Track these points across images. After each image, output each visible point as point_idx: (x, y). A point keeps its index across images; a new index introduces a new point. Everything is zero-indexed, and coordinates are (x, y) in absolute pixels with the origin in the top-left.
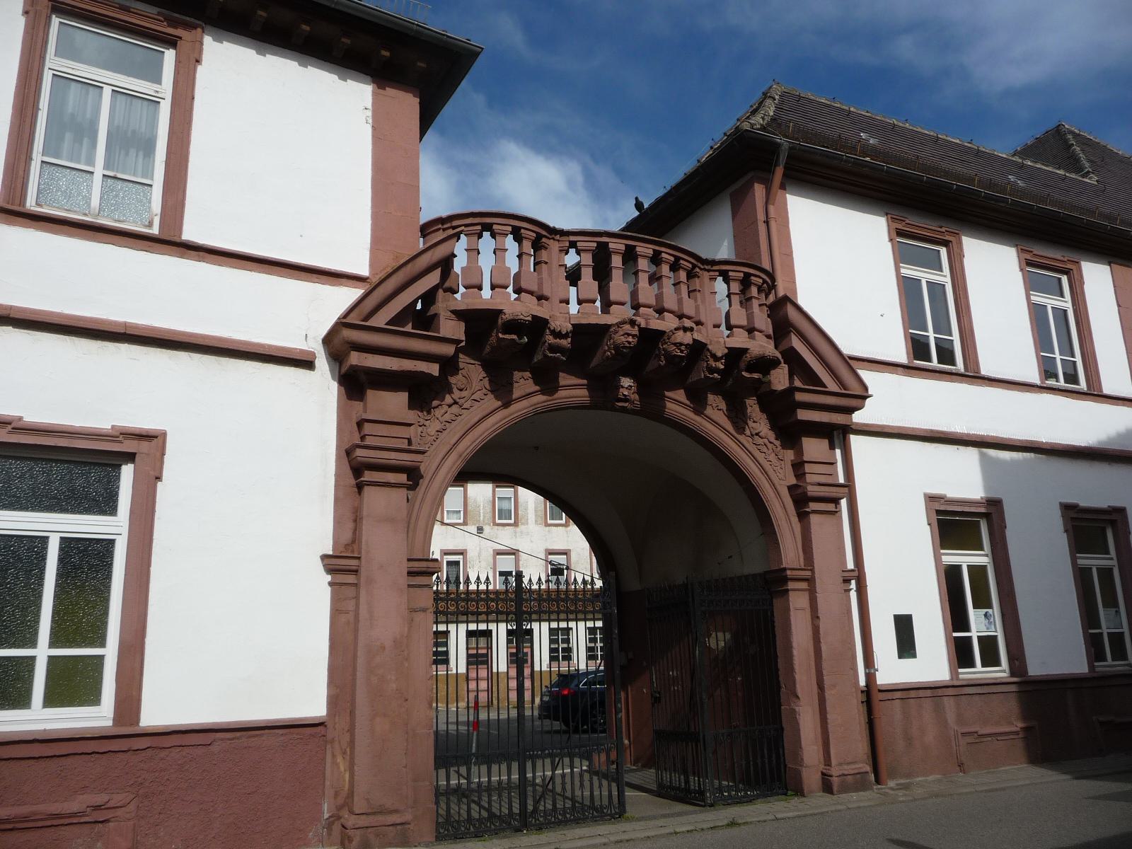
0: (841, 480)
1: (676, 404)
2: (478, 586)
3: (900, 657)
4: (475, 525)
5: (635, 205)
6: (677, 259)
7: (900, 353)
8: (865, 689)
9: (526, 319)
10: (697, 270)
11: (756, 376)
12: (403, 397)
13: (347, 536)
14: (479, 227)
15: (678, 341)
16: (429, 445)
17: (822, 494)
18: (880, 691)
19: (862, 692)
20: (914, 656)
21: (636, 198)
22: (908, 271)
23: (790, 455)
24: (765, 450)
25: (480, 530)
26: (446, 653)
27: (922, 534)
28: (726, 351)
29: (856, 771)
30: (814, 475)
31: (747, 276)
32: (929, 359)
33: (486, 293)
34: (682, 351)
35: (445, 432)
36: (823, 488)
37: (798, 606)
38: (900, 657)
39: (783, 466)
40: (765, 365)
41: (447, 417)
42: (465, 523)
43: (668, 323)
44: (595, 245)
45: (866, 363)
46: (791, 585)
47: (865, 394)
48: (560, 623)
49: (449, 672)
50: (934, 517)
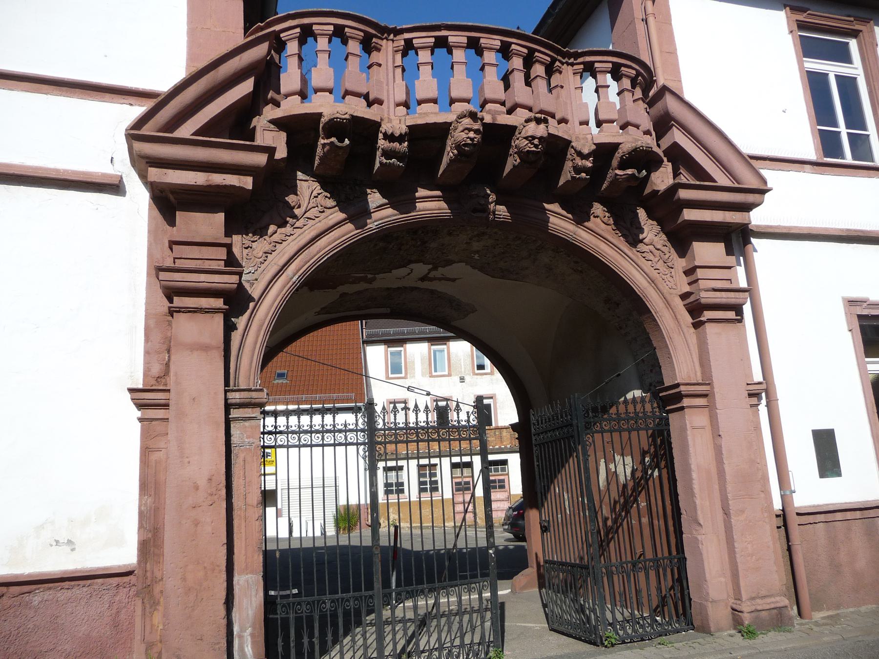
0: (743, 284)
1: (560, 222)
3: (822, 475)
6: (532, 51)
7: (809, 150)
8: (781, 513)
9: (344, 117)
11: (629, 171)
13: (156, 369)
15: (529, 134)
17: (724, 301)
18: (798, 514)
19: (777, 516)
20: (839, 474)
22: (815, 65)
23: (681, 264)
24: (651, 257)
25: (462, 380)
27: (845, 342)
28: (594, 147)
29: (773, 606)
30: (708, 280)
32: (841, 155)
34: (536, 146)
36: (718, 294)
37: (695, 424)
38: (822, 475)
39: (673, 274)
40: (644, 160)
42: (449, 375)
43: (516, 119)
44: (433, 40)
45: (767, 162)
46: (686, 402)
47: (765, 188)
50: (862, 328)
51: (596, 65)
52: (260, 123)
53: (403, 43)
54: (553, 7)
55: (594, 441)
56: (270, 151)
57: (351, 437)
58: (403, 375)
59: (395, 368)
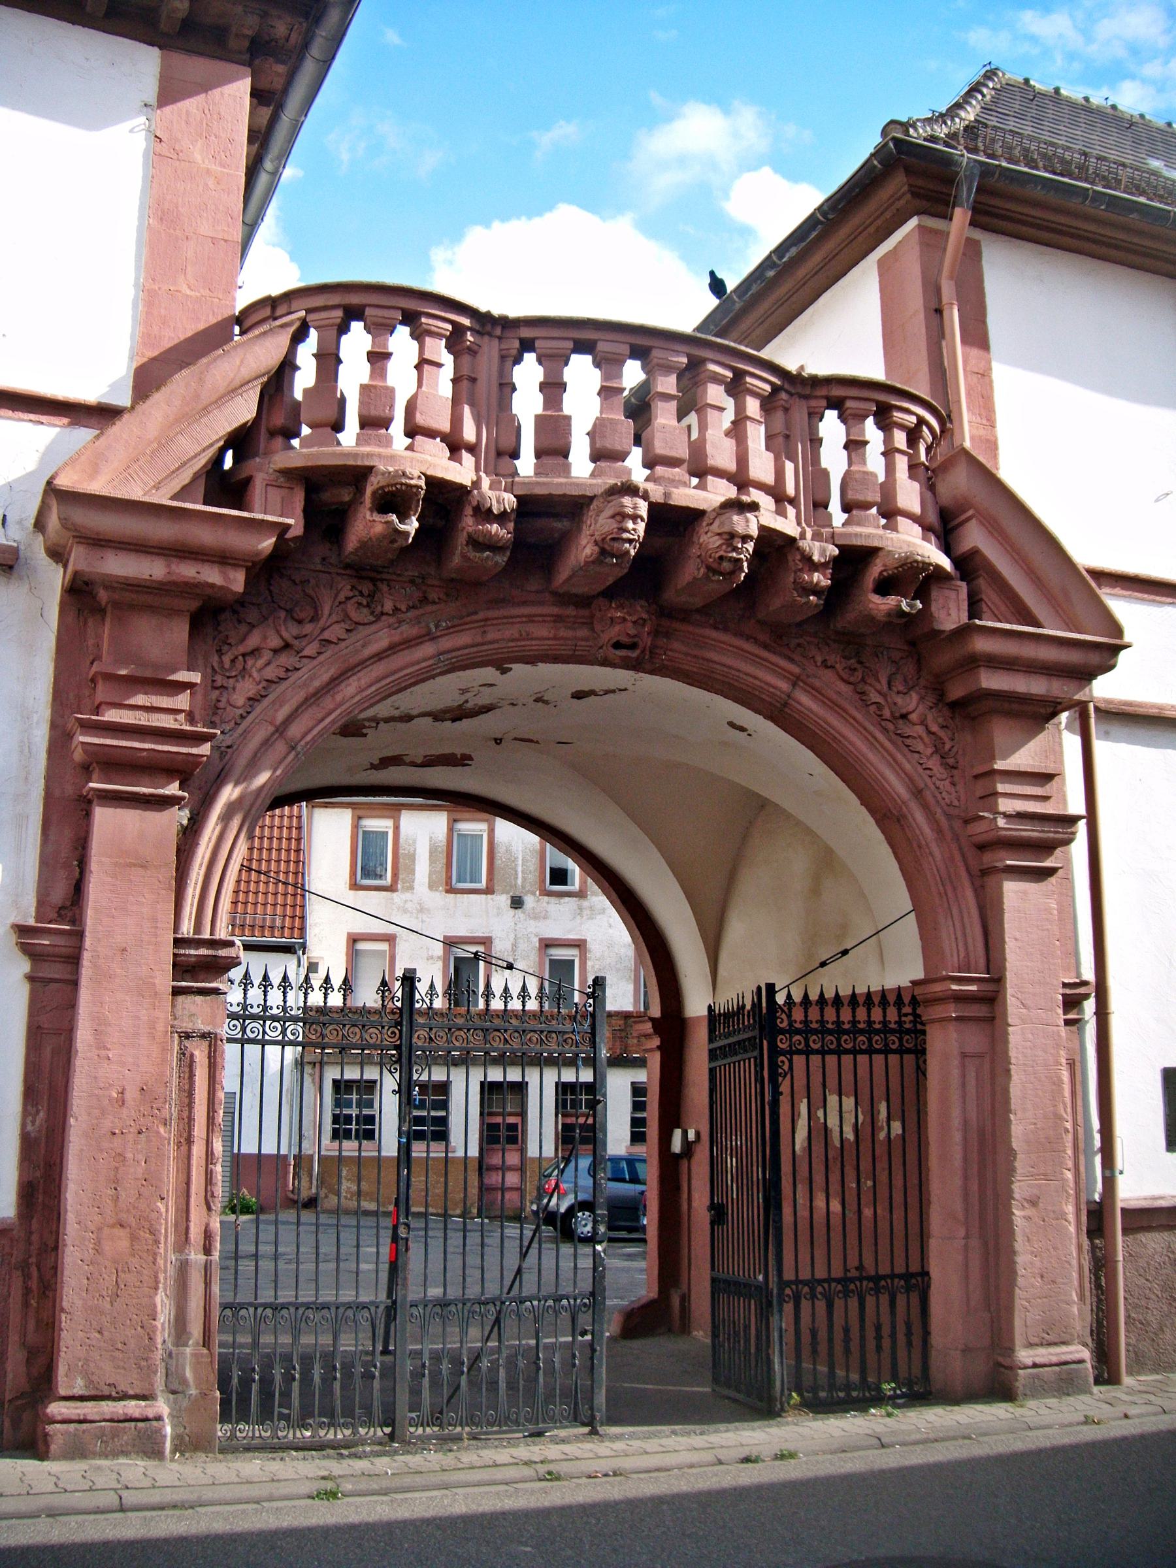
2: (524, 1003)
4: (508, 893)
5: (710, 285)
6: (739, 375)
10: (783, 395)
12: (180, 631)
13: (60, 892)
14: (339, 313)
21: (712, 274)
26: (443, 1121)
33: (349, 437)
35: (266, 702)
39: (956, 779)
40: (915, 579)
41: (271, 673)
42: (489, 891)
48: (346, 1068)
49: (450, 1155)
55: (791, 1068)
57: (372, 1036)
59: (370, 867)
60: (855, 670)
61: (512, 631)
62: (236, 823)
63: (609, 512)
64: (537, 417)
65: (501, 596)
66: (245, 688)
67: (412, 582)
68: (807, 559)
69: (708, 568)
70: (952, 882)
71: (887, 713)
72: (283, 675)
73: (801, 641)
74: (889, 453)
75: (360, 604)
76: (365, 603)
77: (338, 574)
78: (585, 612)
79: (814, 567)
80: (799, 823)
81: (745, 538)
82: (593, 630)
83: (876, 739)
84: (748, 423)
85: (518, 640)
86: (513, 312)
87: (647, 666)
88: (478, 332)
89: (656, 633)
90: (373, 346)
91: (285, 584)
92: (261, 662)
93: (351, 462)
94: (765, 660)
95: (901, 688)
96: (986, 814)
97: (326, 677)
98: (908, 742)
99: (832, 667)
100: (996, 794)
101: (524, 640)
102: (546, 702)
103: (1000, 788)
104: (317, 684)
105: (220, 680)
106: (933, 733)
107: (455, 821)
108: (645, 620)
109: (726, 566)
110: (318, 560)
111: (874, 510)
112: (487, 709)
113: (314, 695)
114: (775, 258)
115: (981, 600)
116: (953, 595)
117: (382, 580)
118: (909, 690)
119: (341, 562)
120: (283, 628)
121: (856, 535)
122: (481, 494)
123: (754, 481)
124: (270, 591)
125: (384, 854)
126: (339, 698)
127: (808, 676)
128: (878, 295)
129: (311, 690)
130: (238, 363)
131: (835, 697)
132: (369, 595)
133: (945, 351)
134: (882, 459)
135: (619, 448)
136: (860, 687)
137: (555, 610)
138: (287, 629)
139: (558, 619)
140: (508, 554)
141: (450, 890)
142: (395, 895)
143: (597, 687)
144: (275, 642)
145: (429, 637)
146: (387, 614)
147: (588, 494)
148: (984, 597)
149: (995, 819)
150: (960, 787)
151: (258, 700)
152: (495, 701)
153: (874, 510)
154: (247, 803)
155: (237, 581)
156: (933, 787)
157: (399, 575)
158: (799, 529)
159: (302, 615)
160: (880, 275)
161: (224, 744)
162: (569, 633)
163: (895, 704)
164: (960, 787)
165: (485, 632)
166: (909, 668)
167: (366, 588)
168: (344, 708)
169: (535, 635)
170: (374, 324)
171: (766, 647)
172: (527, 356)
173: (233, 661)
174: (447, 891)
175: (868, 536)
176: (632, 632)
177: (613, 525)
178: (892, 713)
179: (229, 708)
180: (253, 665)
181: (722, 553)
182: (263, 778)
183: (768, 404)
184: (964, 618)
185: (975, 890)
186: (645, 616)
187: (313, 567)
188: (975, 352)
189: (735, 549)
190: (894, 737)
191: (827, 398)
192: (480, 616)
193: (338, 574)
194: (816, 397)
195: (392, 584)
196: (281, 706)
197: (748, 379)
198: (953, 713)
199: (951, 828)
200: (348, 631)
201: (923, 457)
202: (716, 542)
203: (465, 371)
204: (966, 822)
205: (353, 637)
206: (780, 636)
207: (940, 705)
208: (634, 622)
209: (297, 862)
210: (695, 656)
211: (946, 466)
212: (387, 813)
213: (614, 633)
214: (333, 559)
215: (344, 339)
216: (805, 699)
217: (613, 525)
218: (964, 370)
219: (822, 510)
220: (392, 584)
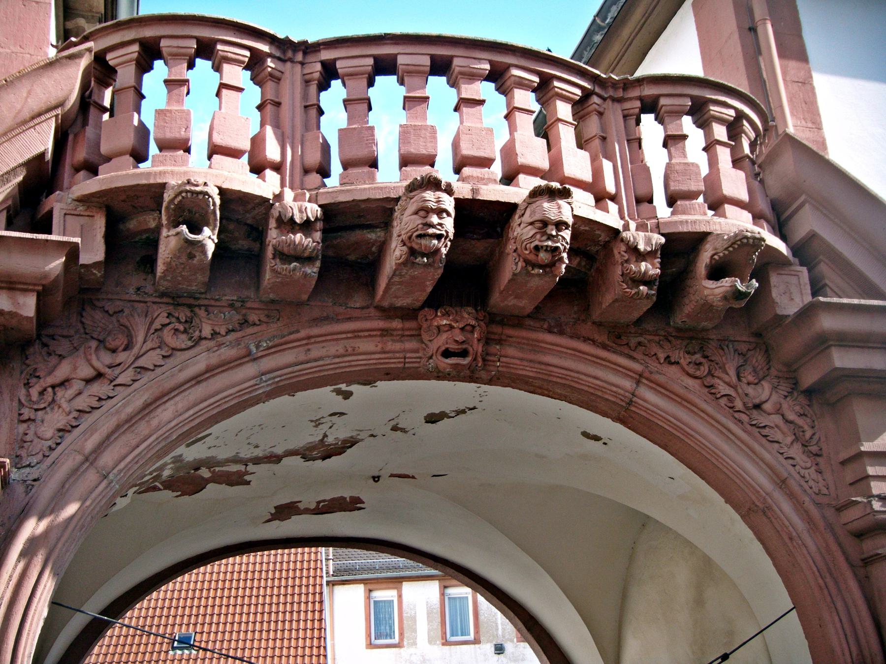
4: (491, 642)
10: (595, 99)
16: (40, 456)
31: (740, 116)
35: (76, 432)
41: (82, 403)
42: (476, 641)
51: (663, 101)
52: (58, 204)
53: (318, 67)
54: (602, 13)
56: (73, 252)
58: (396, 640)
60: (700, 364)
61: (334, 349)
62: (38, 560)
63: (412, 208)
64: (341, 131)
65: (325, 314)
66: (55, 419)
67: (231, 306)
68: (633, 249)
69: (527, 262)
70: (831, 574)
71: (739, 405)
72: (95, 404)
73: (641, 339)
74: (709, 148)
75: (176, 330)
76: (181, 328)
77: (154, 303)
78: (411, 324)
79: (641, 256)
80: (677, 536)
81: (560, 225)
82: (423, 342)
83: (729, 430)
84: (560, 125)
85: (344, 356)
86: (312, 38)
87: (483, 375)
88: (279, 59)
89: (487, 341)
90: (169, 75)
91: (98, 315)
92: (71, 392)
93: (144, 182)
94: (604, 360)
95: (751, 378)
96: (859, 499)
97: (139, 402)
98: (765, 432)
99: (678, 363)
100: (868, 477)
101: (349, 355)
102: (403, 430)
103: (871, 471)
104: (129, 410)
105: (27, 413)
106: (791, 422)
107: (445, 587)
108: (473, 327)
109: (543, 256)
110: (132, 290)
111: (701, 199)
112: (350, 443)
113: (127, 421)
114: (598, 21)
115: (826, 285)
116: (794, 280)
117: (199, 306)
118: (760, 381)
119: (156, 291)
120: (94, 357)
121: (681, 222)
122: (284, 207)
123: (569, 178)
124: (82, 323)
125: (391, 618)
126: (155, 422)
127: (651, 373)
128: (696, 32)
129: (123, 416)
130: (25, 95)
131: (681, 391)
132: (186, 321)
133: (763, 67)
134: (705, 154)
135: (424, 152)
136: (709, 381)
137: (381, 324)
138: (98, 359)
139: (385, 333)
140: (318, 264)
141: (446, 643)
142: (402, 650)
143: (448, 408)
144: (88, 372)
145: (248, 357)
146: (205, 338)
147: (393, 196)
148: (827, 282)
149: (870, 502)
150: (828, 475)
151: (69, 431)
152: (354, 434)
153: (701, 199)
154: (53, 537)
155: (28, 306)
156: (797, 477)
157: (217, 300)
158: (622, 222)
159: (117, 343)
160: (695, 16)
161: (31, 477)
162: (398, 346)
163: (747, 395)
164: (828, 475)
165: (309, 350)
166: (758, 359)
167: (183, 314)
168: (160, 432)
169: (361, 350)
170: (171, 55)
171: (604, 347)
172: (333, 83)
173: (42, 393)
174: (443, 644)
175: (694, 222)
176: (460, 337)
177: (418, 221)
178: (744, 404)
179: (36, 440)
180: (63, 396)
181: (537, 243)
182: (71, 509)
183: (580, 106)
184: (808, 298)
185: (859, 582)
186: (473, 322)
187: (127, 297)
188: (792, 64)
189: (550, 237)
190: (749, 427)
191: (641, 99)
192: (303, 333)
193: (154, 303)
194: (631, 99)
195: (210, 309)
196: (92, 435)
197: (556, 84)
198: (810, 400)
199: (824, 517)
200: (164, 357)
201: (747, 150)
202: (530, 231)
203: (270, 96)
204: (839, 509)
205: (171, 362)
206: (617, 335)
207: (796, 394)
208: (462, 329)
209: (320, 629)
210: (531, 361)
211: (772, 158)
212: (391, 585)
213: (442, 341)
214: (149, 289)
215: (146, 76)
216: (650, 396)
217: (418, 221)
218: (784, 80)
219: (645, 206)
220: (210, 309)
